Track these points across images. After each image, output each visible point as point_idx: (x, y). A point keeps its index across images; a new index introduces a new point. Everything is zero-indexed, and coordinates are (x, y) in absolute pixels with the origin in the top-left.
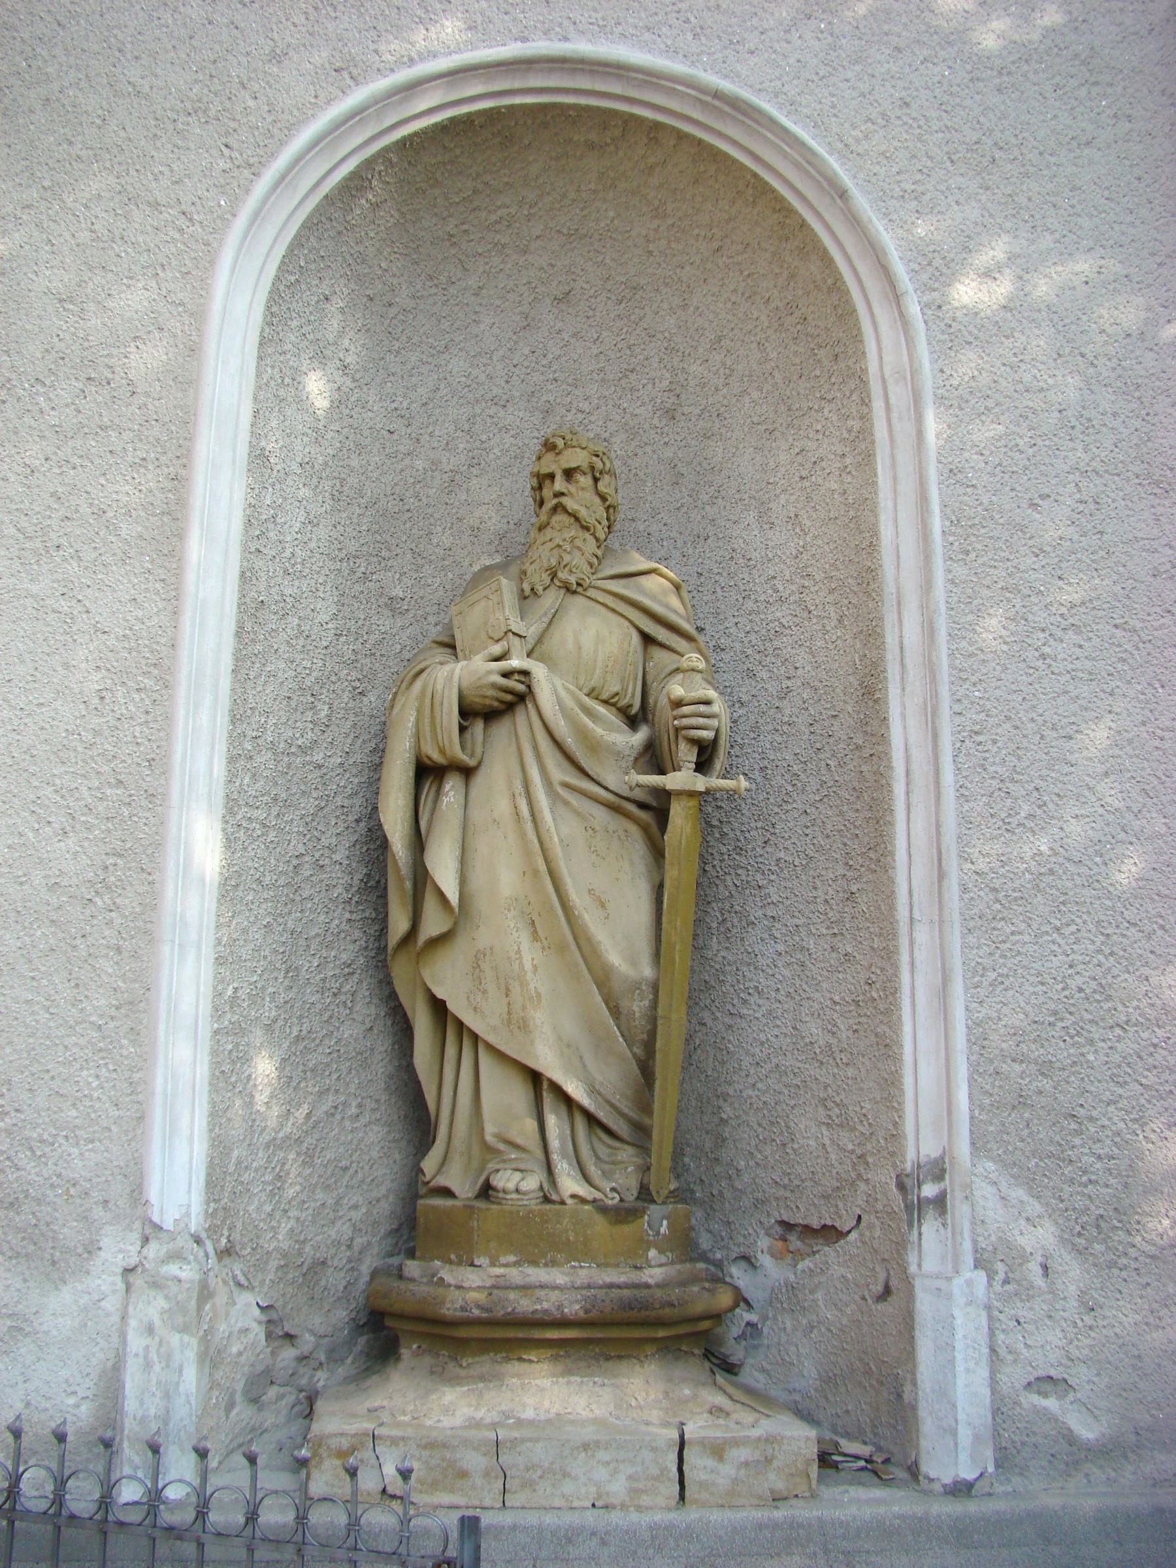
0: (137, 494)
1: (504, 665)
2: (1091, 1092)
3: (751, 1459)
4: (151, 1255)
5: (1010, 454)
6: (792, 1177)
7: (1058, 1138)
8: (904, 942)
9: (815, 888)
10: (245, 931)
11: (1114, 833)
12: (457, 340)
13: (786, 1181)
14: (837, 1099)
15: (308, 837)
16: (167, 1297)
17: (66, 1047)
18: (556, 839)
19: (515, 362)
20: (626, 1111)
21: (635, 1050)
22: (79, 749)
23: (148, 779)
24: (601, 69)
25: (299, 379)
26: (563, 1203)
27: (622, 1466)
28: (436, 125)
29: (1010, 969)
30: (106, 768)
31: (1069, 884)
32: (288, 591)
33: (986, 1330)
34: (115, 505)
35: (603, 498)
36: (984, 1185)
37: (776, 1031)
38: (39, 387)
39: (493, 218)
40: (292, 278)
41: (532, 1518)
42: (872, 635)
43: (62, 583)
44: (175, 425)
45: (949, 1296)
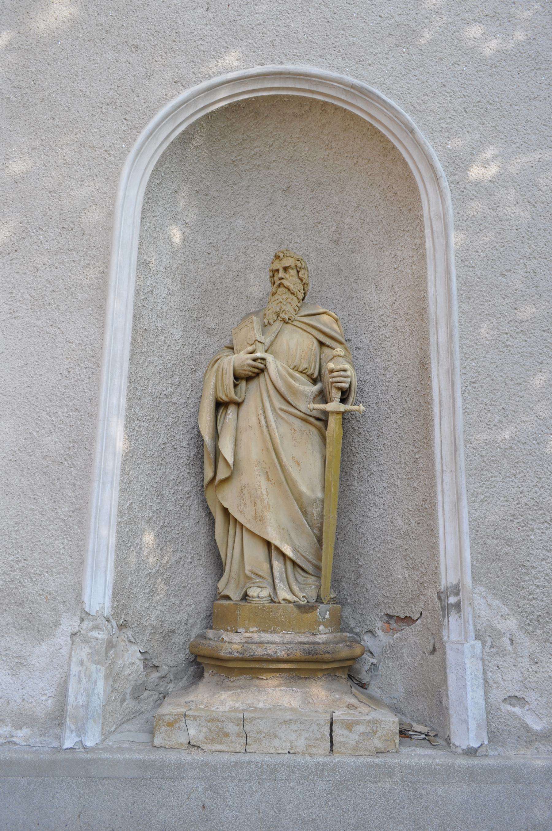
0: (85, 280)
1: (253, 355)
2: (533, 554)
3: (365, 731)
4: (84, 627)
5: (491, 251)
6: (391, 593)
7: (516, 576)
8: (439, 481)
9: (400, 457)
10: (137, 477)
11: (543, 429)
12: (239, 211)
13: (388, 595)
14: (411, 556)
15: (169, 435)
16: (90, 647)
17: (49, 530)
18: (277, 434)
19: (266, 221)
20: (311, 560)
21: (315, 531)
22: (58, 394)
23: (89, 408)
24: (298, 77)
25: (163, 229)
26: (280, 603)
27: (303, 733)
28: (222, 107)
29: (490, 494)
30: (70, 403)
31: (520, 454)
32: (159, 325)
33: (482, 671)
34: (75, 285)
35: (301, 280)
36: (479, 598)
37: (383, 524)
38: (40, 232)
39: (253, 152)
40: (158, 181)
41: (258, 758)
42: (424, 339)
43: (51, 320)
44: (102, 248)
45: (463, 653)
